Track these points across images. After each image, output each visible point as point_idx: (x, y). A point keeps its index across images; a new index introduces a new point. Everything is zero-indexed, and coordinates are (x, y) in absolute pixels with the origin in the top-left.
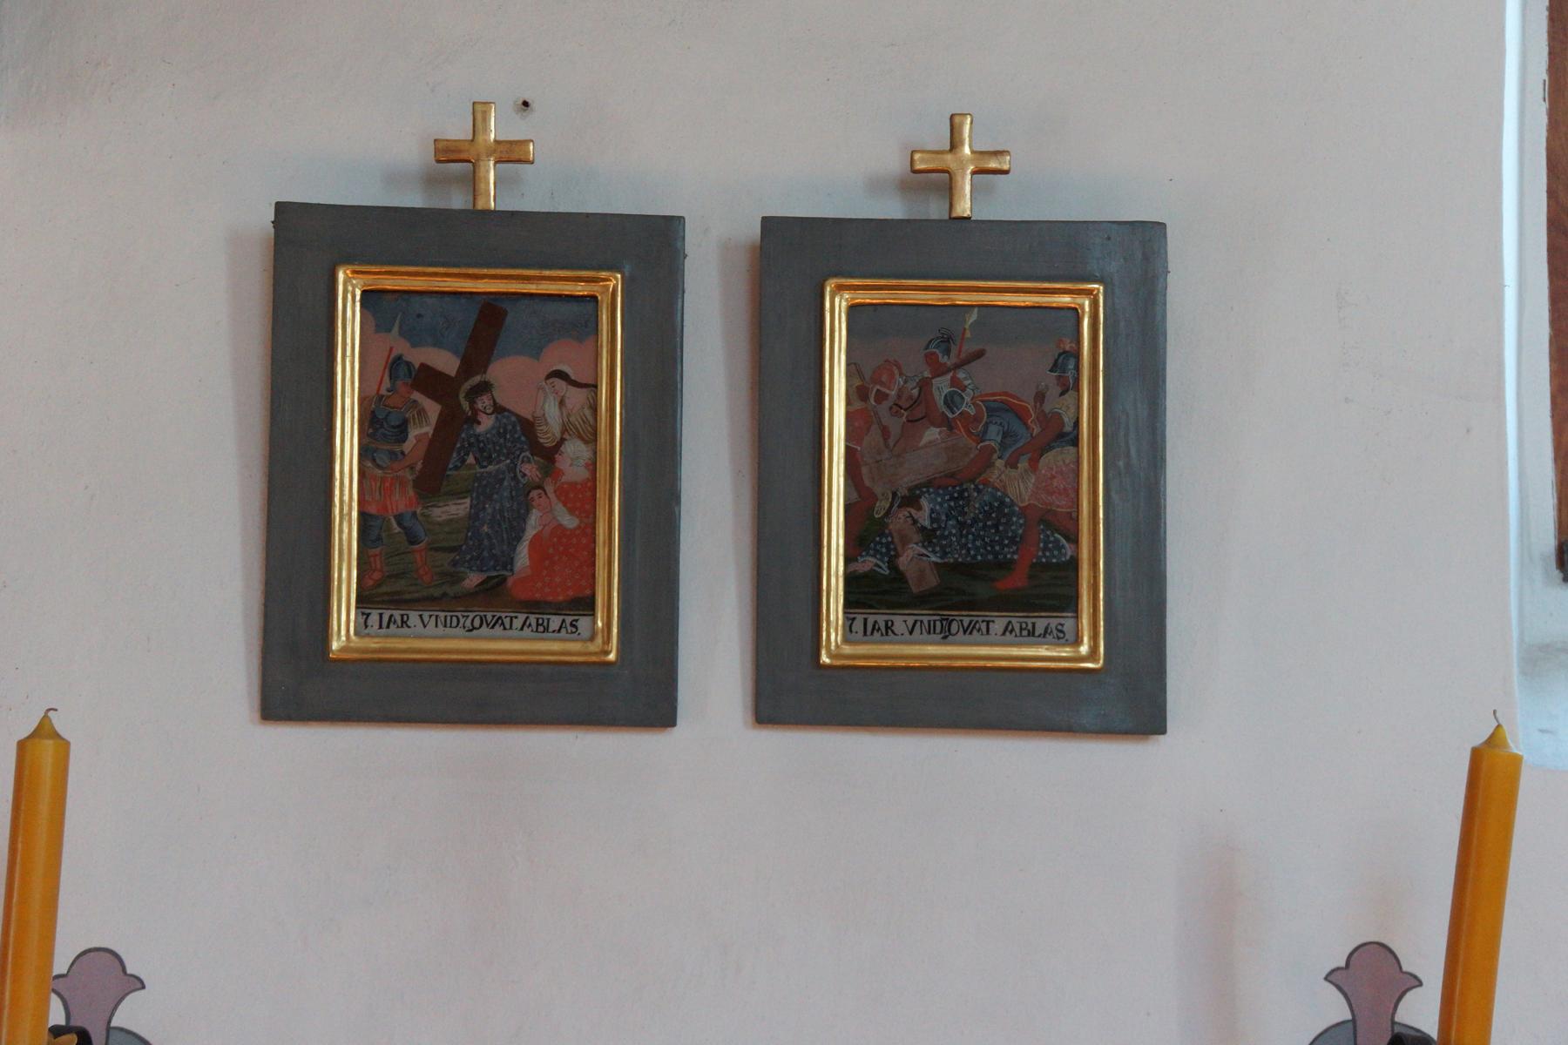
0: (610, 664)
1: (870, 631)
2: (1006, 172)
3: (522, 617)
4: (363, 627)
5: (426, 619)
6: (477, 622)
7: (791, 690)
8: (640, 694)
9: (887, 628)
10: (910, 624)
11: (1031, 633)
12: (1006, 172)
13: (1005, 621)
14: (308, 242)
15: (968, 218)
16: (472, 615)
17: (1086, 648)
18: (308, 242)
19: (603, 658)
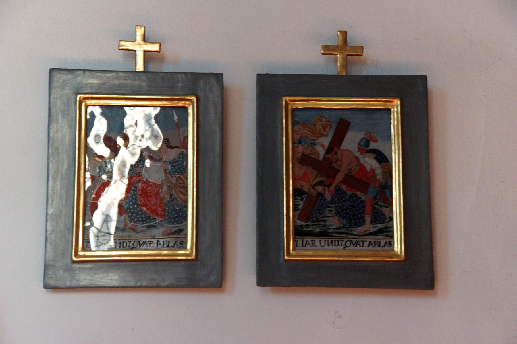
7: (273, 273)
11: (168, 246)
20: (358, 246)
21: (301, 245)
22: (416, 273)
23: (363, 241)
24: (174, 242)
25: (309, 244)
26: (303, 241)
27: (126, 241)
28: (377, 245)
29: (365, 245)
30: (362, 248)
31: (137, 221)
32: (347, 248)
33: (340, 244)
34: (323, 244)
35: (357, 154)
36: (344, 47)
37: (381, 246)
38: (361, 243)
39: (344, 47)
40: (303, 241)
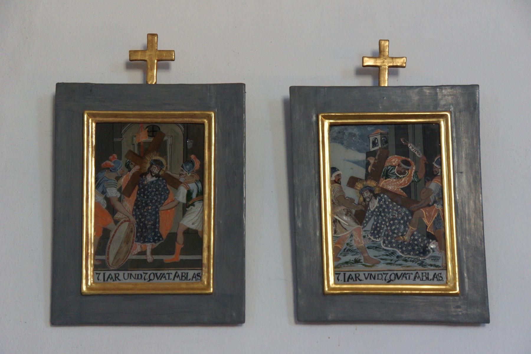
0: (210, 294)
1: (348, 279)
2: (404, 67)
3: (174, 272)
4: (96, 279)
5: (366, 275)
6: (393, 277)
7: (313, 306)
8: (226, 308)
9: (116, 277)
10: (366, 275)
11: (427, 278)
12: (404, 67)
13: (175, 271)
14: (71, 100)
15: (388, 87)
16: (149, 272)
17: (208, 282)
18: (71, 100)
19: (207, 292)
20: (163, 279)
21: (102, 280)
22: (470, 309)
23: (169, 274)
24: (433, 275)
25: (165, 277)
26: (104, 274)
27: (382, 272)
28: (184, 278)
29: (411, 278)
30: (167, 281)
31: (410, 251)
32: (151, 281)
33: (143, 278)
34: (126, 277)
35: (413, 163)
36: (148, 56)
37: (188, 279)
38: (167, 276)
39: (148, 56)
40: (104, 274)
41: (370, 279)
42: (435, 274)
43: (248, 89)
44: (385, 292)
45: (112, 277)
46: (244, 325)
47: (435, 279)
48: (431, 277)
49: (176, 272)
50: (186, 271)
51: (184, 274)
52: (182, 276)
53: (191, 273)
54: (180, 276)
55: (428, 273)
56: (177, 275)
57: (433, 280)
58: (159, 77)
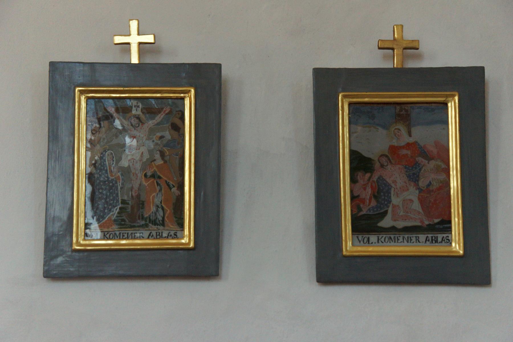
11: (436, 242)
18: (328, 83)
41: (416, 242)
42: (443, 237)
43: (488, 74)
44: (139, 247)
45: (153, 235)
46: (491, 286)
47: (443, 242)
48: (440, 239)
49: (151, 233)
50: (436, 235)
51: (434, 238)
52: (432, 240)
53: (440, 237)
54: (430, 240)
55: (437, 237)
56: (151, 235)
57: (168, 237)
58: (411, 64)
